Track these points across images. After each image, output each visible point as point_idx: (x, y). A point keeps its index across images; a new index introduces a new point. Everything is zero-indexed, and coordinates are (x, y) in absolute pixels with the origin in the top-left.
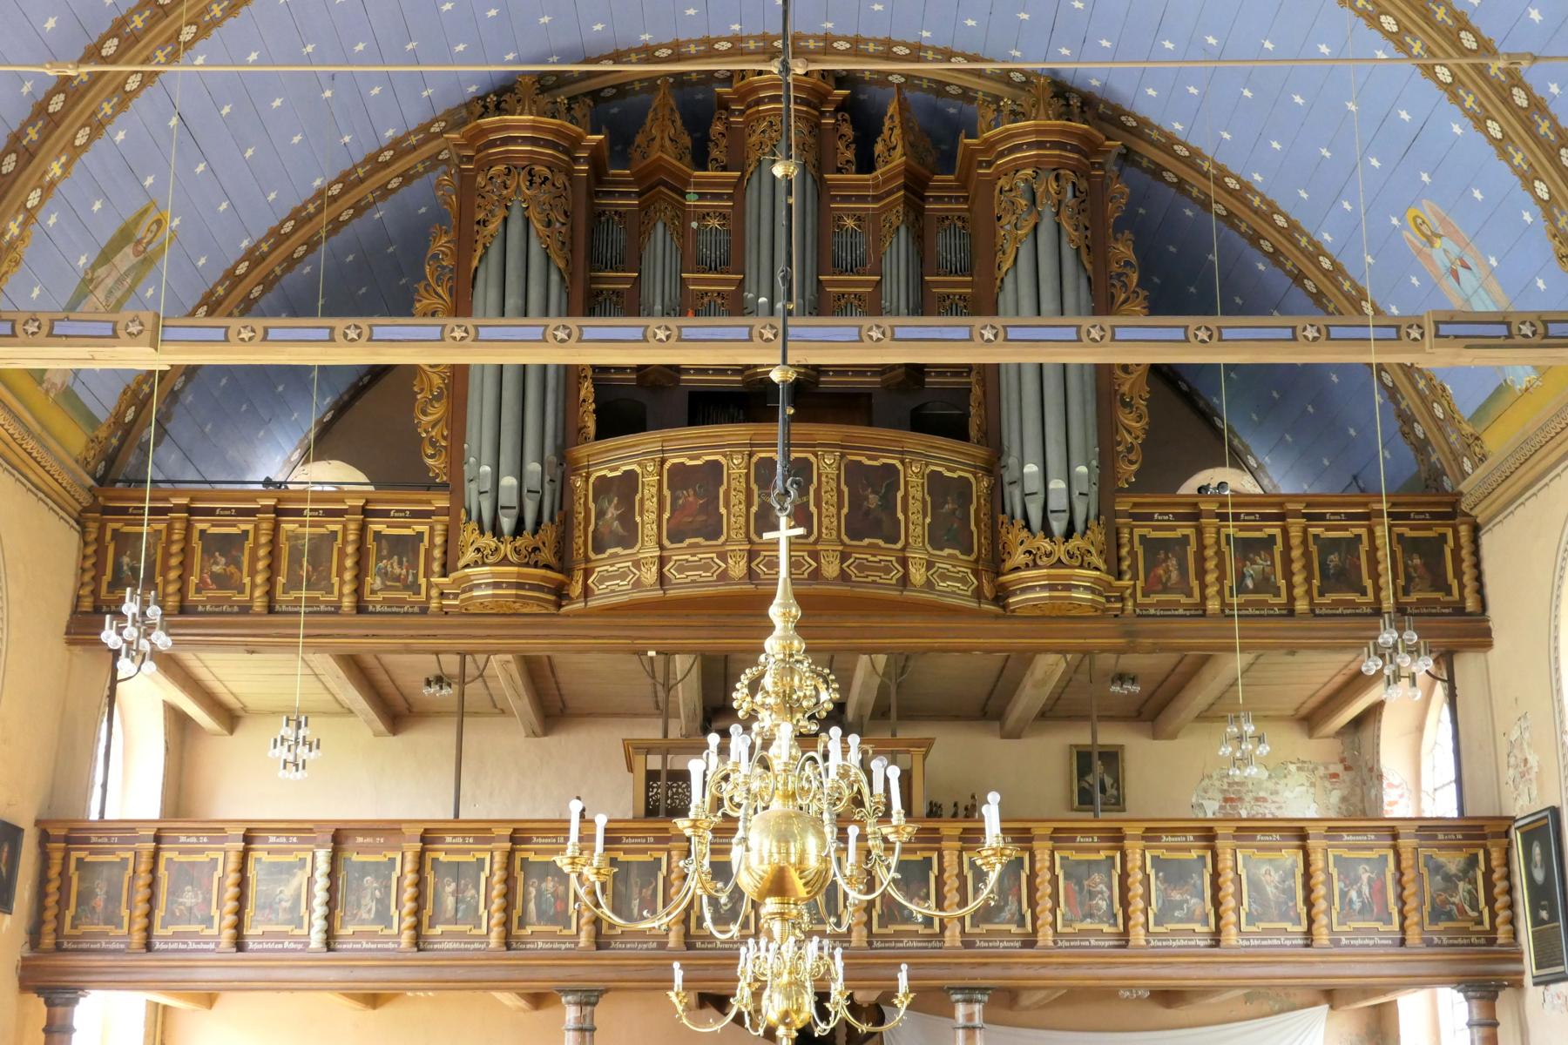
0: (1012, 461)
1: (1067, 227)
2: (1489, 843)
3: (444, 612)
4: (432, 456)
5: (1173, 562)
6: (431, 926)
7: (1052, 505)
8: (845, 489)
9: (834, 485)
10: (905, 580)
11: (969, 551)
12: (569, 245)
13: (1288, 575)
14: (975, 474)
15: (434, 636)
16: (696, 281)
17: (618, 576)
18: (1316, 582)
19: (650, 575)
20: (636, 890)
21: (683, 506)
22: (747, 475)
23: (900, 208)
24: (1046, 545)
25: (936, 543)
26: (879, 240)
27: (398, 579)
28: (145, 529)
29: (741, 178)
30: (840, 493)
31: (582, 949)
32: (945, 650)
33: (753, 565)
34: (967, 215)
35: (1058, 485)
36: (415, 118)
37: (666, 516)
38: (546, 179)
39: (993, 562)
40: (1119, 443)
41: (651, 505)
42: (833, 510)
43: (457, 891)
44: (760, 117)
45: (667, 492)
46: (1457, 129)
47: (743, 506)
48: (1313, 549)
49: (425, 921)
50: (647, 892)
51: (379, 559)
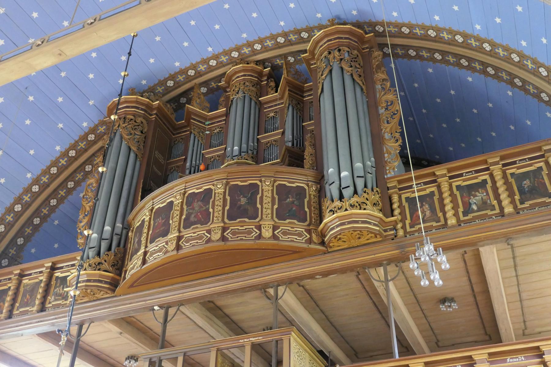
8: (228, 198)
10: (260, 237)
13: (497, 196)
18: (517, 197)
25: (281, 215)
28: (422, 226)
38: (132, 119)
41: (219, 203)
48: (512, 180)
51: (55, 288)
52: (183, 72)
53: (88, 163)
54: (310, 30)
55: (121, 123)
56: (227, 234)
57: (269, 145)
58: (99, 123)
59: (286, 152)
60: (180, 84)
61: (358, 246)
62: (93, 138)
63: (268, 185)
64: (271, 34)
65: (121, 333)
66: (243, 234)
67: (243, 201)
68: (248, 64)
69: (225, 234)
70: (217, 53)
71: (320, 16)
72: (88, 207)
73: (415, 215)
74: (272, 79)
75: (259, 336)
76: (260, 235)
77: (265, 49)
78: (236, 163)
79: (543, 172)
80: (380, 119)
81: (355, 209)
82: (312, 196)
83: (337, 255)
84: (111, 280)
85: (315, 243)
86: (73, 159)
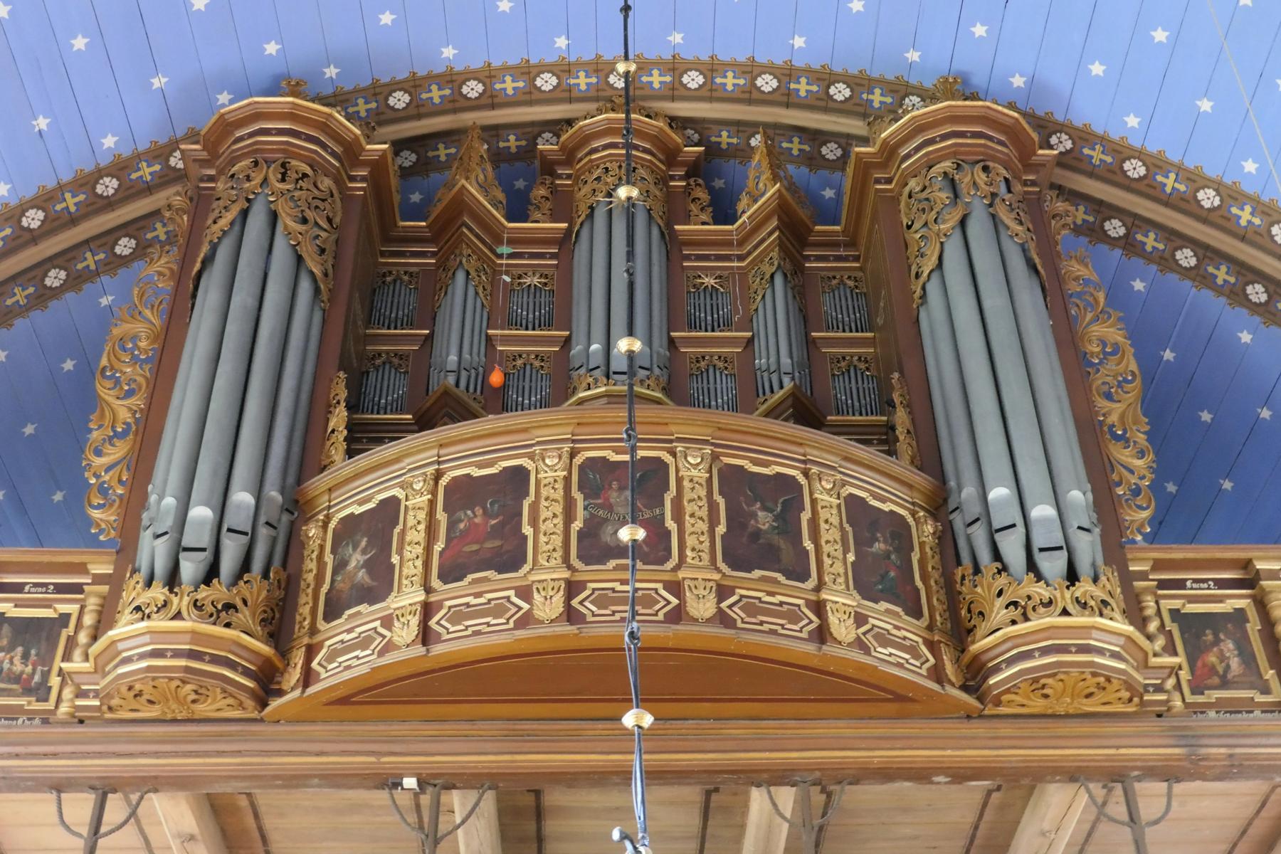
0: (969, 492)
1: (1006, 218)
4: (99, 507)
5: (1229, 646)
7: (1038, 542)
8: (721, 501)
9: (703, 493)
10: (822, 634)
11: (918, 615)
12: (333, 253)
14: (913, 514)
15: (55, 755)
16: (507, 340)
17: (354, 646)
19: (406, 632)
21: (465, 533)
22: (567, 480)
23: (775, 254)
24: (1040, 591)
26: (747, 300)
27: (17, 679)
29: (568, 232)
30: (713, 507)
32: (886, 774)
33: (575, 603)
34: (859, 274)
35: (1042, 511)
36: (147, 133)
37: (439, 547)
38: (305, 175)
39: (957, 627)
40: (1119, 484)
41: (417, 535)
42: (703, 526)
44: (592, 166)
45: (441, 516)
47: (559, 521)
52: (452, 79)
53: (60, 261)
54: (900, 90)
55: (271, 176)
57: (703, 364)
58: (147, 152)
59: (790, 402)
60: (422, 110)
61: (1067, 716)
62: (111, 192)
63: (551, 467)
65: (192, 838)
66: (771, 615)
67: (764, 520)
68: (648, 116)
69: (575, 603)
70: (573, 59)
71: (917, 60)
72: (124, 410)
73: (1199, 664)
74: (700, 181)
77: (710, 93)
78: (606, 395)
80: (1090, 387)
81: (1090, 616)
82: (928, 550)
83: (1006, 729)
84: (259, 668)
85: (953, 685)
86: (27, 236)
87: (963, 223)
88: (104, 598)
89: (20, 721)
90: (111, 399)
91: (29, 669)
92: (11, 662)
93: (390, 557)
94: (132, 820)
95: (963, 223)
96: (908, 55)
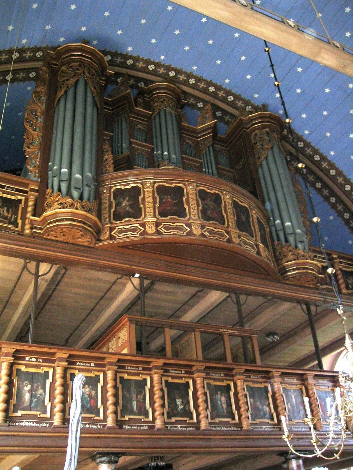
2: (106, 369)
3: (33, 235)
6: (15, 411)
20: (134, 396)
24: (70, 201)
27: (6, 218)
31: (110, 428)
38: (94, 75)
43: (30, 391)
46: (195, 68)
49: (11, 407)
50: (140, 397)
52: (126, 57)
56: (160, 229)
60: (135, 68)
64: (211, 81)
69: (159, 228)
75: (236, 330)
76: (145, 231)
79: (20, 205)
87: (76, 83)
88: (36, 197)
89: (10, 232)
90: (31, 130)
91: (10, 215)
92: (3, 212)
93: (139, 204)
94: (25, 269)
95: (76, 83)
96: (255, 95)
